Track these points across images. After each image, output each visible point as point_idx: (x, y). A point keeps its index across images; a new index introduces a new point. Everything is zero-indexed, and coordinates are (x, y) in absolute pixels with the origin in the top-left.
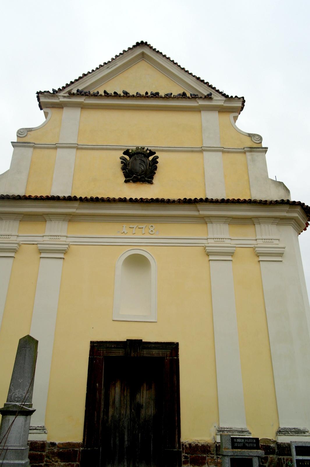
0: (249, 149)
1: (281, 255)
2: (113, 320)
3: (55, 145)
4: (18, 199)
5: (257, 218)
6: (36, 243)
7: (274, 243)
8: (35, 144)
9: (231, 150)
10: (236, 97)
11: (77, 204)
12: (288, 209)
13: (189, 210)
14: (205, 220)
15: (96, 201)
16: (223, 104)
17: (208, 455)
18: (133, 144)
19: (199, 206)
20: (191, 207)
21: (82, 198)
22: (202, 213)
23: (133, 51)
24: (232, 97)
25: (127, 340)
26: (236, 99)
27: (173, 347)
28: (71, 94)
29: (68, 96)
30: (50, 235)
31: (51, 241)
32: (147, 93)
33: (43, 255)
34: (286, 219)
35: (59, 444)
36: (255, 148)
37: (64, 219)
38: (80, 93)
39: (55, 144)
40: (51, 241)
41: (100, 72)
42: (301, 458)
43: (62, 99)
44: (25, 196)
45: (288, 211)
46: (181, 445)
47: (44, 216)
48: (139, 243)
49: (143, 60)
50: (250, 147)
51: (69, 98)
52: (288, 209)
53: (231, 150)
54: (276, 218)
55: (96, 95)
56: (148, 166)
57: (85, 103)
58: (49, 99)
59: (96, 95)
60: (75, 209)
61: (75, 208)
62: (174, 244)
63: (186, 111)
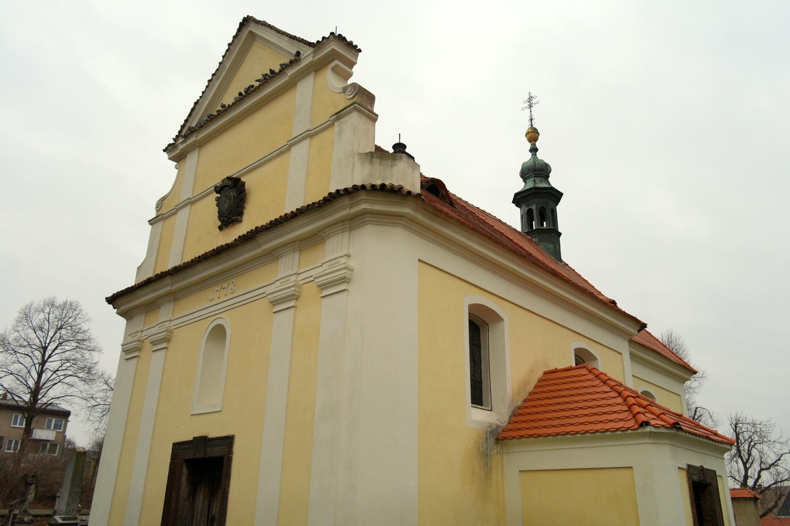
0: (335, 116)
1: (344, 280)
4: (271, 227)
5: (322, 229)
8: (191, 199)
9: (241, 172)
10: (324, 38)
11: (168, 280)
12: (347, 202)
13: (322, 219)
14: (273, 255)
15: (228, 249)
18: (218, 180)
19: (261, 239)
20: (251, 245)
22: (264, 247)
23: (238, 39)
26: (325, 41)
28: (186, 137)
29: (184, 140)
30: (328, 260)
31: (337, 266)
32: (240, 94)
33: (325, 293)
34: (256, 258)
36: (341, 111)
37: (343, 229)
38: (201, 126)
40: (337, 266)
41: (211, 90)
43: (181, 147)
44: (161, 272)
45: (351, 204)
46: (65, 522)
47: (319, 233)
48: (223, 304)
50: (334, 113)
52: (347, 202)
53: (241, 172)
54: (342, 221)
55: (226, 109)
56: (232, 201)
57: (199, 140)
58: (174, 152)
59: (226, 109)
60: (348, 209)
61: (346, 208)
62: (219, 305)
63: (209, 141)
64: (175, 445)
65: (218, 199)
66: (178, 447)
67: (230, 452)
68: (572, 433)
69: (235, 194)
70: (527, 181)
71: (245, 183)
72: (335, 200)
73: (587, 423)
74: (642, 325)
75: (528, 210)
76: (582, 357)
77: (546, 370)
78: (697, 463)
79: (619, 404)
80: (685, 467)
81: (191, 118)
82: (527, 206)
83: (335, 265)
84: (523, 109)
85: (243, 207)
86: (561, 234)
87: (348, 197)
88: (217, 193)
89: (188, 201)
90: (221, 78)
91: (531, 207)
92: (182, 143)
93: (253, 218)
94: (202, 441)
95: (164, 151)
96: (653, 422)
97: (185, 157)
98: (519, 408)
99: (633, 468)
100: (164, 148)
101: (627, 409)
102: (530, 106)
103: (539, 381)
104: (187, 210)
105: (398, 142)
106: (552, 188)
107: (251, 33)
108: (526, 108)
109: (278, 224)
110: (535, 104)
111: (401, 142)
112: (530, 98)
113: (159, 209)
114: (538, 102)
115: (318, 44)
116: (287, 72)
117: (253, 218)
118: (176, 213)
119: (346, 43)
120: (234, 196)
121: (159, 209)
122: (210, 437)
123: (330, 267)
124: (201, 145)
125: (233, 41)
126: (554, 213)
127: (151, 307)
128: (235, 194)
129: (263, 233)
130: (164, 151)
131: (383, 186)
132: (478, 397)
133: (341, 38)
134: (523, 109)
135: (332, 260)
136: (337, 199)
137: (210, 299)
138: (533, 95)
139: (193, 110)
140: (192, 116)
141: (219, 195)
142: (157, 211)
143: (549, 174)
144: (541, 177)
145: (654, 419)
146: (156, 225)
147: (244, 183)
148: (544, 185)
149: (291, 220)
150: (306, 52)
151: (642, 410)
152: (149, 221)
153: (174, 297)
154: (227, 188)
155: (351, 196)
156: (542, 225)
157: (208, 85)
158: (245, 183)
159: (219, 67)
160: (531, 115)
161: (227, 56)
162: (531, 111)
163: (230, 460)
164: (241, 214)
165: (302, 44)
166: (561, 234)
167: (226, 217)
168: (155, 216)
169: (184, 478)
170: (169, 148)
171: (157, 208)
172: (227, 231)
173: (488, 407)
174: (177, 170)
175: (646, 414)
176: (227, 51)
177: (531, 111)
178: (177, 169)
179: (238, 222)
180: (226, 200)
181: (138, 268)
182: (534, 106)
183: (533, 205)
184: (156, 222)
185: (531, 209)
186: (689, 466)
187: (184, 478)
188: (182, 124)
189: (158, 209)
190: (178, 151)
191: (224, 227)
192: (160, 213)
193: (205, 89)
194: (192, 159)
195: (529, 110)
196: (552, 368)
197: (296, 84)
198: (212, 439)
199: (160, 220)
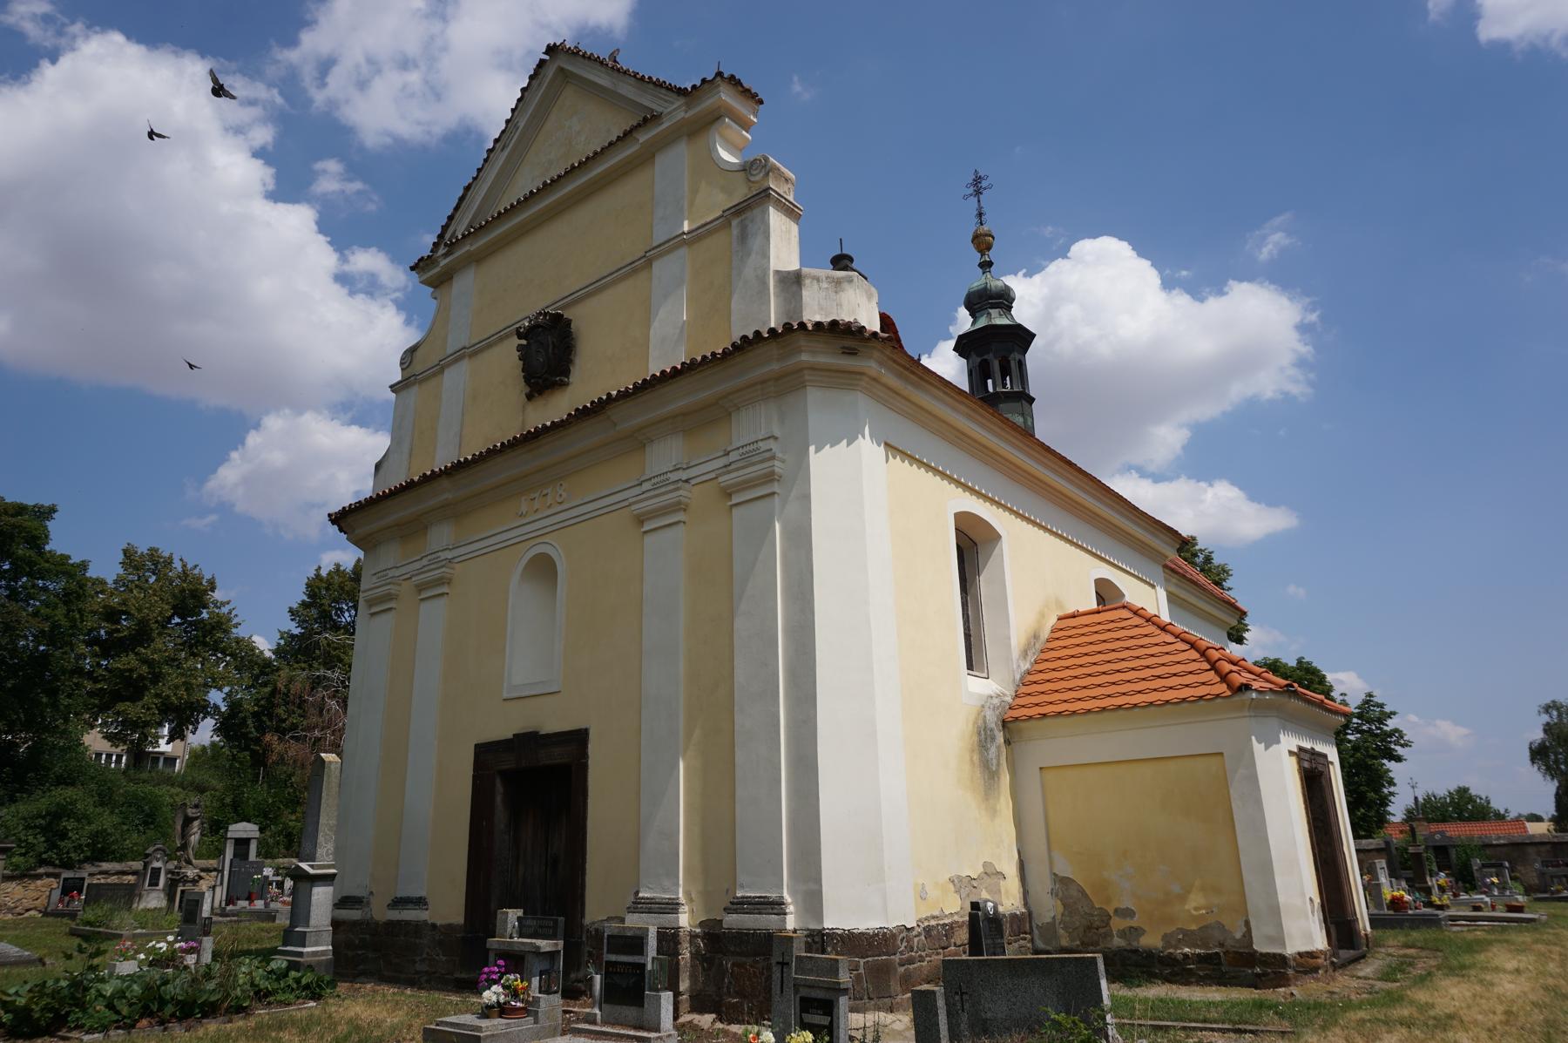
2: (504, 700)
3: (439, 364)
6: (408, 576)
7: (762, 450)
16: (682, 114)
17: (1425, 965)
19: (615, 413)
21: (1234, 279)
24: (694, 87)
25: (514, 735)
26: (706, 86)
27: (578, 739)
28: (452, 247)
29: (448, 251)
35: (441, 926)
39: (437, 363)
42: (613, 958)
43: (443, 263)
49: (568, 82)
51: (451, 254)
56: (550, 350)
64: (477, 746)
65: (520, 348)
66: (485, 754)
67: (584, 754)
68: (1209, 697)
69: (555, 340)
70: (977, 315)
71: (571, 320)
72: (751, 348)
73: (1148, 691)
74: (1183, 542)
75: (980, 363)
76: (1106, 593)
77: (1061, 614)
78: (1307, 745)
79: (1194, 660)
80: (1296, 750)
81: (459, 213)
82: (979, 355)
83: (751, 454)
84: (965, 197)
85: (570, 361)
86: (1033, 399)
87: (774, 343)
88: (520, 338)
89: (463, 351)
90: (511, 145)
91: (986, 357)
92: (446, 255)
93: (587, 384)
94: (529, 741)
95: (412, 268)
96: (1256, 685)
97: (451, 278)
98: (1029, 673)
99: (1225, 754)
100: (412, 265)
101: (1209, 667)
102: (978, 193)
103: (1052, 632)
104: (465, 365)
105: (840, 252)
106: (1020, 327)
107: (561, 69)
108: (971, 195)
109: (646, 389)
110: (985, 189)
111: (844, 252)
112: (978, 180)
113: (408, 367)
114: (990, 187)
115: (694, 91)
116: (638, 137)
117: (587, 384)
118: (442, 371)
119: (740, 89)
120: (553, 342)
121: (408, 367)
122: (542, 732)
123: (743, 457)
124: (478, 259)
125: (529, 84)
126: (1021, 365)
127: (412, 530)
128: (555, 340)
129: (617, 403)
130: (412, 268)
131: (834, 323)
132: (973, 661)
133: (734, 81)
134: (965, 197)
135: (746, 445)
136: (755, 346)
137: (520, 513)
138: (981, 174)
139: (462, 199)
140: (461, 209)
141: (524, 342)
142: (402, 369)
143: (1012, 303)
144: (1000, 308)
145: (1254, 680)
146: (404, 394)
147: (569, 322)
148: (1004, 321)
149: (670, 381)
150: (673, 103)
151: (1235, 668)
152: (391, 387)
153: (453, 512)
154: (540, 329)
155: (778, 340)
156: (1004, 386)
157: (488, 157)
158: (571, 320)
159: (506, 128)
160: (980, 208)
161: (519, 109)
162: (979, 201)
163: (584, 768)
164: (567, 373)
165: (663, 91)
166: (1033, 399)
167: (540, 378)
168: (400, 379)
169: (499, 799)
170: (421, 264)
171: (401, 364)
172: (539, 402)
173: (983, 672)
174: (435, 301)
175: (1242, 674)
176: (519, 100)
177: (979, 201)
178: (435, 298)
179: (564, 385)
180: (541, 350)
181: (378, 466)
182: (984, 192)
183: (989, 353)
184: (403, 388)
185: (986, 360)
186: (1301, 749)
187: (499, 799)
188: (444, 224)
189: (405, 366)
190: (437, 270)
191: (536, 395)
192: (410, 372)
193: (483, 165)
194: (465, 283)
195: (976, 199)
196: (1070, 610)
197: (653, 156)
198: (548, 736)
199: (413, 384)
